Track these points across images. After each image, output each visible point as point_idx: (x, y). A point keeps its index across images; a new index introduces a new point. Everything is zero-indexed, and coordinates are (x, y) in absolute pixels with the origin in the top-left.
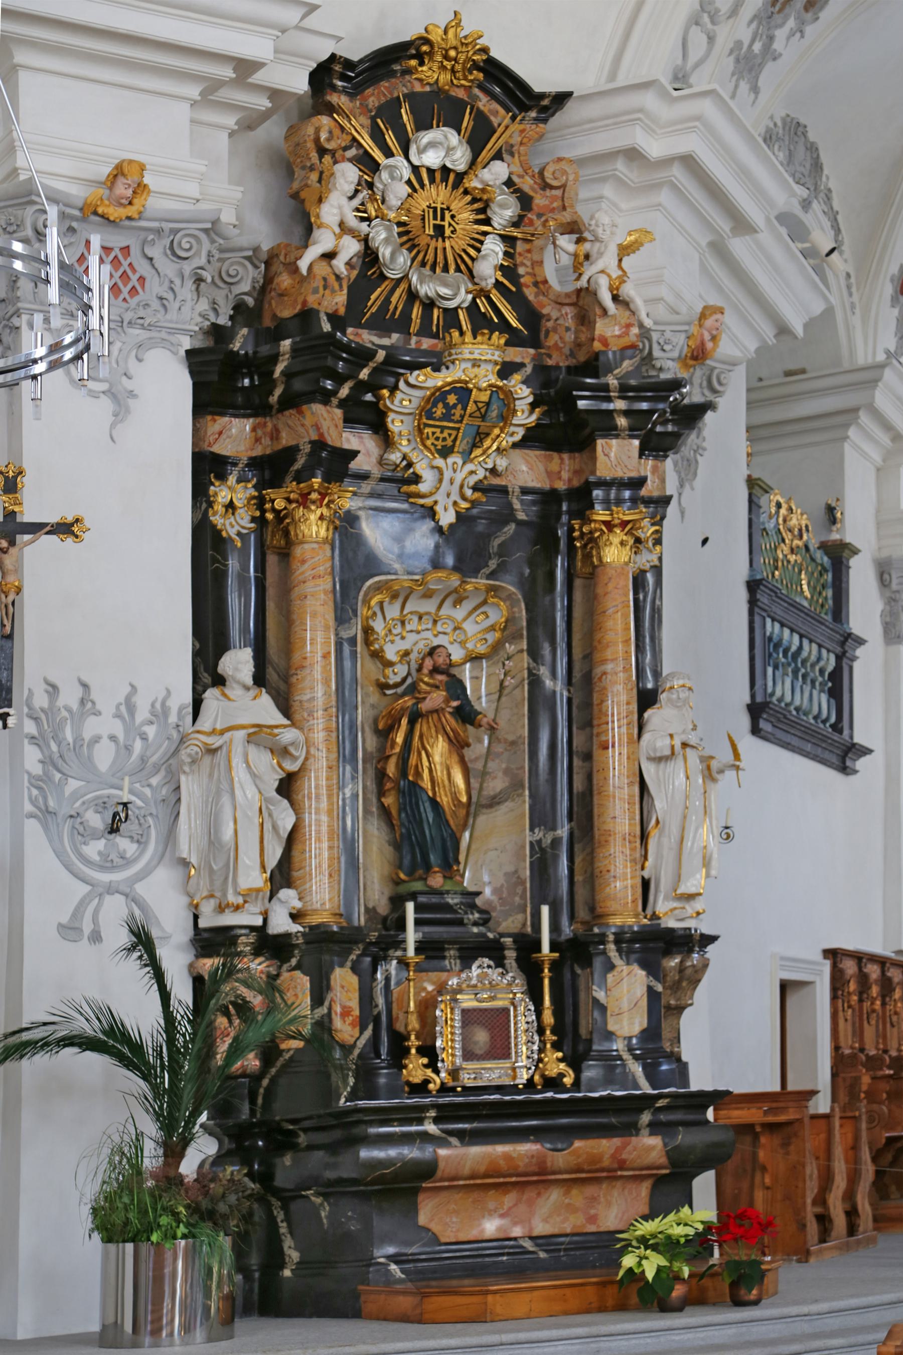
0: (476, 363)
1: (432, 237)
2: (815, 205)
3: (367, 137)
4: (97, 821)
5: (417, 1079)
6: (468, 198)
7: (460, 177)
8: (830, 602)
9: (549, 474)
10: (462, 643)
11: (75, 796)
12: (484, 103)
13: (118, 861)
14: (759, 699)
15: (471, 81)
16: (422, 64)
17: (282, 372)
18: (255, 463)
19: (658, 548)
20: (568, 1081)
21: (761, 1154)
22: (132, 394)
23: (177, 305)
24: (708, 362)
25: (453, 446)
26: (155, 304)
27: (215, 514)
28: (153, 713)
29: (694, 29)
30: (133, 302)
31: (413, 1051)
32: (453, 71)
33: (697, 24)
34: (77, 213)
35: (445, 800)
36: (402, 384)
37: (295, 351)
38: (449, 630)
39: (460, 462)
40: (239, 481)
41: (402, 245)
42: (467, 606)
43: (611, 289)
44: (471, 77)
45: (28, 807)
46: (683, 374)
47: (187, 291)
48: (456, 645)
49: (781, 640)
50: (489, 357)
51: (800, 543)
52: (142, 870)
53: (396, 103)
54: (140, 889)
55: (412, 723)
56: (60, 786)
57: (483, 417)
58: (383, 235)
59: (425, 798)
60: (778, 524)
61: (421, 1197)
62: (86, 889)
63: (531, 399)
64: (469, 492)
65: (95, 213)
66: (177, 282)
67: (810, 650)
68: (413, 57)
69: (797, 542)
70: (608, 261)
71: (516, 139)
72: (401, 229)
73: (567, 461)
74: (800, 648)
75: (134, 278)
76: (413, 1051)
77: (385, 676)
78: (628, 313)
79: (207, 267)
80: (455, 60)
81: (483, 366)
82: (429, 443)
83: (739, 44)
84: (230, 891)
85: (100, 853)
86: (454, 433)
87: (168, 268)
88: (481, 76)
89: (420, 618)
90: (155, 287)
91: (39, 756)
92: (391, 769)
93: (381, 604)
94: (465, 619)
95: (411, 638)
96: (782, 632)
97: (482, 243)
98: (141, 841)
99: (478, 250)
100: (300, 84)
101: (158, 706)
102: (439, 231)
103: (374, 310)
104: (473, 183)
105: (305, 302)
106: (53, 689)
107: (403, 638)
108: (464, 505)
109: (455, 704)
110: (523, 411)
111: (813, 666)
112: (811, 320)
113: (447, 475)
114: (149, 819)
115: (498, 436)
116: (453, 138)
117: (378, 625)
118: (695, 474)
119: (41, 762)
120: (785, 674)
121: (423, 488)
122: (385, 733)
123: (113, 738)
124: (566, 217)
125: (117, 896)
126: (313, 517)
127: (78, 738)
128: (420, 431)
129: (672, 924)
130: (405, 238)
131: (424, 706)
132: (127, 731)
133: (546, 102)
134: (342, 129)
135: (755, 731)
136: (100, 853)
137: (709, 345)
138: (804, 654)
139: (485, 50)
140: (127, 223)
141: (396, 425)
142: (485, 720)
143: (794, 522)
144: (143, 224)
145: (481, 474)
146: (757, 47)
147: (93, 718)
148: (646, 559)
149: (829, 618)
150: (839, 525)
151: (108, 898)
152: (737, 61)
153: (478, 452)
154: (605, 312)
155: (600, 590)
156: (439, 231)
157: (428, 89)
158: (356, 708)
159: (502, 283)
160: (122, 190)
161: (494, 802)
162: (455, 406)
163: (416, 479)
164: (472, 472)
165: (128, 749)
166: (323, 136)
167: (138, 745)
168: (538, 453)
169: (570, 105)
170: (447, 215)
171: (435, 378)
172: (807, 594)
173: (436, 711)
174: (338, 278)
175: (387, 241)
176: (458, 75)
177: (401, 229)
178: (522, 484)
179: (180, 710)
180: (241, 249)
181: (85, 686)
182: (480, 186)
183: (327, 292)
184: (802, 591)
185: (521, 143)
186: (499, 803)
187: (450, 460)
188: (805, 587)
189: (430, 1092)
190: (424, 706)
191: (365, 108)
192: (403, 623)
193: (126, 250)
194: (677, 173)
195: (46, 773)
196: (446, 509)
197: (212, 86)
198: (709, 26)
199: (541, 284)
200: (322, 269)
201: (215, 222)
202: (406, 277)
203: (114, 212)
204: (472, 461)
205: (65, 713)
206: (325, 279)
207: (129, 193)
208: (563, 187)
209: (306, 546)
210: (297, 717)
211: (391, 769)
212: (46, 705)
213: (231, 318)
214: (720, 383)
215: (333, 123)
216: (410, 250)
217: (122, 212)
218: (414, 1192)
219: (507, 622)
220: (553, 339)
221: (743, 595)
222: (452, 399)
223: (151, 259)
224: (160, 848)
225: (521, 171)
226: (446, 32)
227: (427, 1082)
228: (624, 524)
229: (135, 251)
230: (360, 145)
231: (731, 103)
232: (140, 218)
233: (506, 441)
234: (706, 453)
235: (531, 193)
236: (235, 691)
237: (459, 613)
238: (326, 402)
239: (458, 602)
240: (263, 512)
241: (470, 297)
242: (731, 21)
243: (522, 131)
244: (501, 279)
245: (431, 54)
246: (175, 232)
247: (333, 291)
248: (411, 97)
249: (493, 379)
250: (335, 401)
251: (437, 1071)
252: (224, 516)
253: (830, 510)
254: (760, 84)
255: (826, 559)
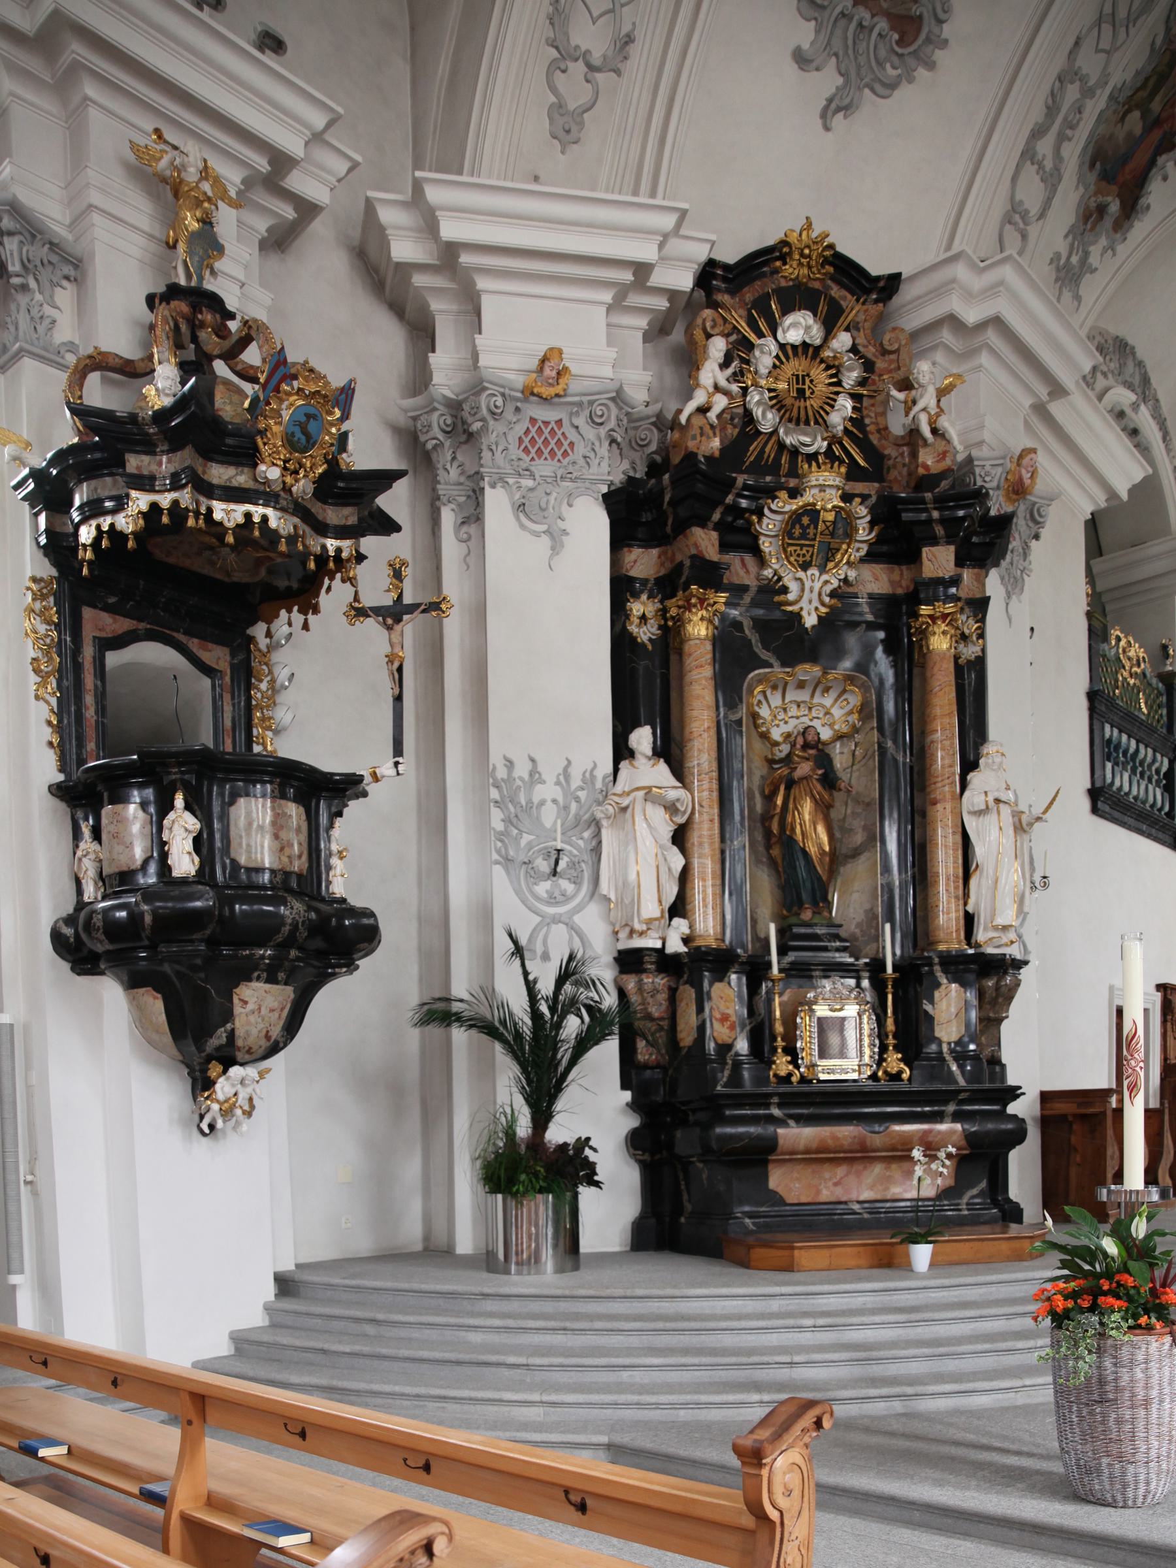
0: (822, 488)
1: (796, 398)
2: (1143, 407)
3: (744, 324)
4: (544, 866)
5: (783, 1073)
6: (823, 366)
7: (817, 349)
8: (1165, 719)
9: (892, 582)
10: (831, 725)
11: (530, 846)
12: (836, 291)
13: (561, 898)
14: (1098, 784)
15: (824, 274)
16: (785, 264)
17: (669, 503)
18: (659, 581)
19: (980, 641)
20: (905, 1076)
21: (1073, 1138)
22: (564, 532)
23: (597, 461)
24: (1029, 497)
25: (811, 561)
26: (582, 462)
27: (631, 624)
28: (584, 780)
29: (1008, 227)
30: (565, 461)
31: (780, 1050)
32: (810, 267)
33: (1010, 223)
34: (519, 395)
35: (813, 850)
36: (766, 511)
37: (673, 481)
38: (821, 716)
39: (817, 573)
40: (649, 598)
41: (772, 407)
42: (833, 694)
43: (930, 424)
44: (823, 271)
45: (495, 856)
46: (1009, 509)
47: (604, 450)
48: (827, 728)
49: (1119, 743)
50: (831, 483)
51: (1139, 671)
52: (578, 905)
53: (766, 297)
54: (577, 919)
55: (788, 788)
56: (517, 840)
57: (832, 535)
58: (757, 398)
59: (797, 848)
60: (1117, 652)
61: (770, 1167)
62: (538, 919)
63: (868, 518)
64: (827, 600)
65: (532, 394)
66: (597, 444)
67: (1145, 753)
68: (777, 259)
69: (1135, 669)
70: (928, 399)
71: (861, 317)
72: (772, 394)
73: (905, 573)
74: (1137, 751)
75: (566, 444)
76: (780, 1050)
77: (773, 754)
78: (944, 443)
79: (617, 429)
80: (809, 256)
81: (828, 491)
82: (792, 559)
83: (1058, 256)
84: (636, 920)
85: (547, 892)
86: (810, 549)
87: (590, 432)
88: (831, 269)
89: (799, 706)
90: (581, 449)
91: (502, 816)
92: (775, 828)
93: (764, 693)
94: (832, 706)
95: (793, 722)
96: (1120, 737)
97: (835, 401)
98: (577, 881)
99: (832, 407)
100: (685, 281)
101: (587, 775)
102: (801, 392)
103: (752, 459)
104: (827, 353)
105: (686, 448)
106: (510, 764)
107: (786, 723)
108: (824, 610)
109: (820, 772)
110: (864, 529)
111: (1150, 766)
112: (1134, 486)
113: (808, 584)
114: (583, 865)
115: (847, 551)
116: (810, 320)
117: (764, 712)
118: (1022, 589)
119: (503, 820)
120: (1125, 769)
121: (791, 597)
122: (769, 798)
123: (554, 801)
124: (900, 375)
125: (561, 925)
126: (695, 619)
127: (530, 802)
128: (785, 551)
129: (990, 950)
130: (774, 402)
131: (798, 774)
132: (565, 795)
133: (882, 284)
134: (725, 320)
135: (1095, 810)
136: (547, 892)
137: (1027, 482)
138: (1141, 755)
139: (831, 247)
140: (557, 400)
141: (766, 545)
142: (843, 785)
143: (1132, 653)
144: (569, 399)
145: (835, 583)
146: (1074, 259)
147: (539, 786)
148: (970, 651)
149: (1164, 731)
150: (1170, 660)
151: (554, 927)
152: (1058, 269)
153: (830, 565)
154: (925, 440)
155: (928, 674)
156: (801, 392)
157: (791, 283)
158: (742, 776)
159: (852, 432)
160: (549, 372)
161: (855, 854)
162: (808, 526)
163: (785, 590)
164: (826, 582)
165: (566, 808)
166: (708, 325)
167: (574, 806)
168: (882, 566)
169: (903, 287)
170: (807, 380)
171: (790, 504)
172: (1145, 710)
173: (806, 778)
174: (712, 427)
175: (759, 403)
176: (814, 270)
177: (772, 394)
178: (870, 591)
179: (604, 778)
180: (648, 417)
181: (533, 760)
182: (831, 355)
183: (704, 438)
184: (1140, 709)
185: (865, 320)
186: (859, 854)
187: (809, 572)
188: (1143, 705)
189: (791, 1083)
190: (798, 774)
191: (743, 303)
192: (785, 710)
193: (559, 423)
194: (992, 336)
195: (506, 828)
196: (809, 614)
197: (622, 292)
198: (1021, 225)
199: (883, 431)
200: (698, 421)
201: (619, 392)
202: (775, 432)
203: (546, 391)
204: (827, 572)
205: (519, 783)
206: (701, 428)
207: (554, 374)
208: (897, 351)
209: (691, 643)
210: (687, 781)
211: (775, 828)
212: (505, 777)
213: (647, 474)
214: (1040, 516)
215: (716, 315)
216: (779, 410)
217: (552, 391)
218: (765, 1163)
219: (862, 705)
220: (894, 474)
221: (1084, 703)
222: (805, 520)
223: (577, 427)
224: (591, 887)
225: (865, 342)
226: (800, 235)
227: (790, 1075)
228: (944, 616)
229: (566, 422)
230: (739, 331)
231: (1029, 270)
232: (565, 395)
233: (855, 556)
234: (1032, 574)
235: (874, 359)
236: (641, 761)
237: (828, 701)
238: (703, 526)
239: (827, 690)
240: (666, 620)
241: (825, 443)
242: (1041, 222)
243: (866, 311)
244: (851, 428)
245: (790, 254)
246: (591, 403)
247: (708, 437)
248: (780, 292)
249: (837, 502)
250: (711, 525)
251: (797, 1067)
252: (639, 626)
253: (1165, 648)
254: (1080, 293)
255: (1160, 685)
